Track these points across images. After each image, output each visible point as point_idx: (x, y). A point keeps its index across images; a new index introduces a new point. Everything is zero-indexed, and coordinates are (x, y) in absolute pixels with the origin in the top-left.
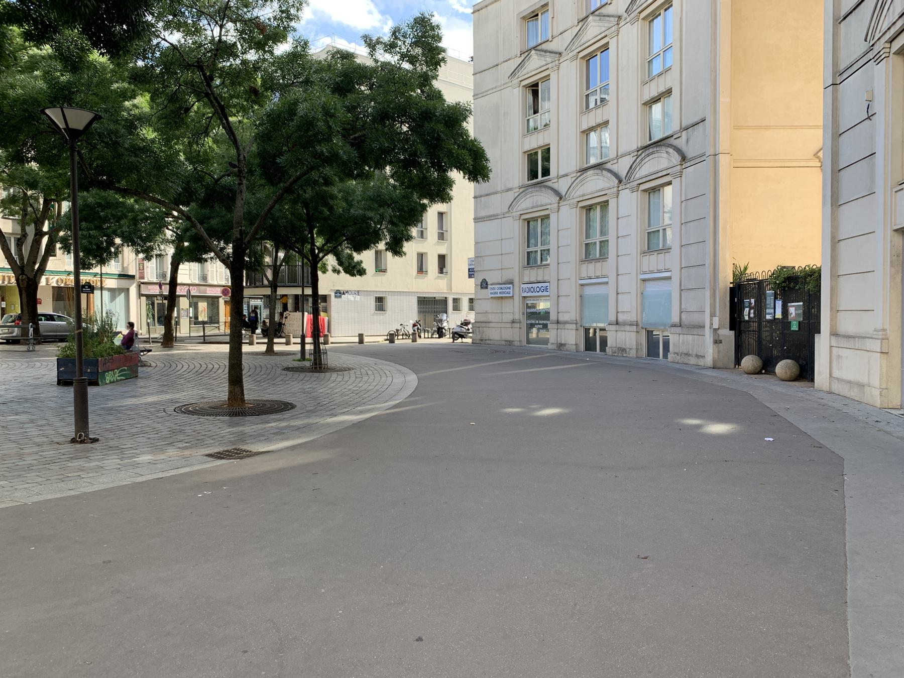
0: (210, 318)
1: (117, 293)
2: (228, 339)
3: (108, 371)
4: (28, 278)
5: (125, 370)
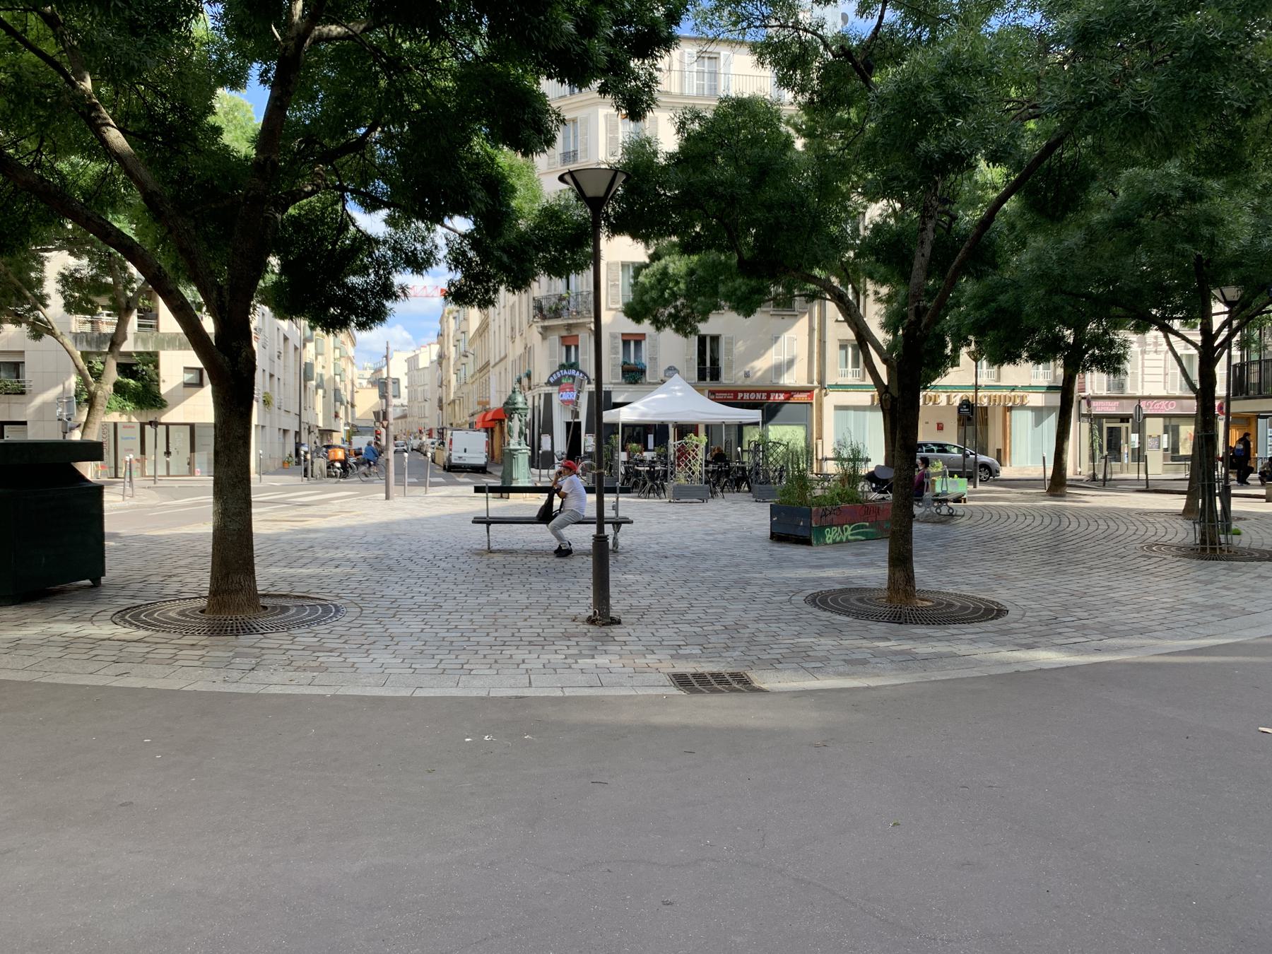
0: (491, 455)
1: (1045, 413)
2: (1185, 486)
3: (831, 526)
4: (892, 397)
5: (863, 527)
